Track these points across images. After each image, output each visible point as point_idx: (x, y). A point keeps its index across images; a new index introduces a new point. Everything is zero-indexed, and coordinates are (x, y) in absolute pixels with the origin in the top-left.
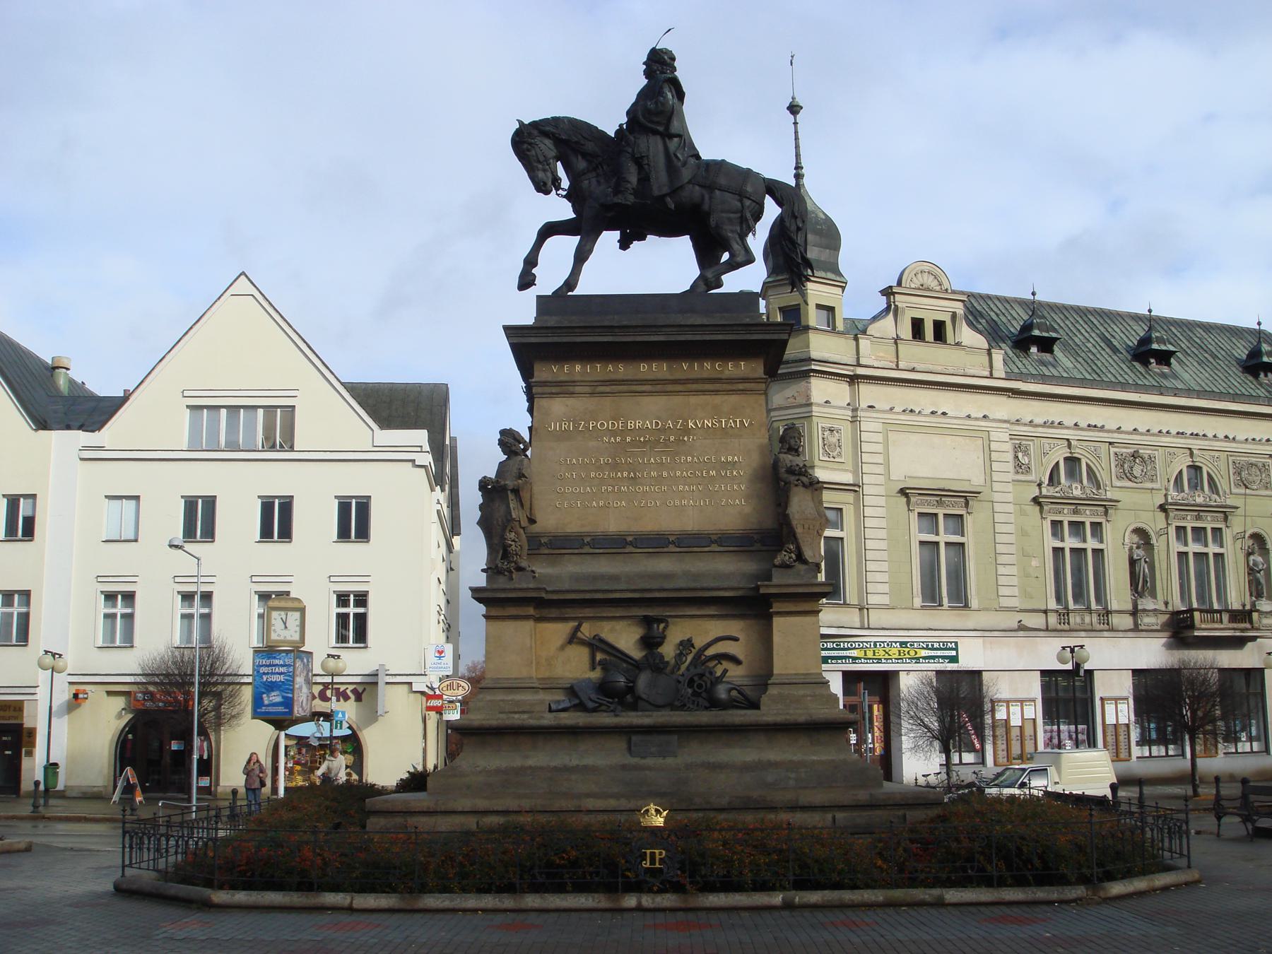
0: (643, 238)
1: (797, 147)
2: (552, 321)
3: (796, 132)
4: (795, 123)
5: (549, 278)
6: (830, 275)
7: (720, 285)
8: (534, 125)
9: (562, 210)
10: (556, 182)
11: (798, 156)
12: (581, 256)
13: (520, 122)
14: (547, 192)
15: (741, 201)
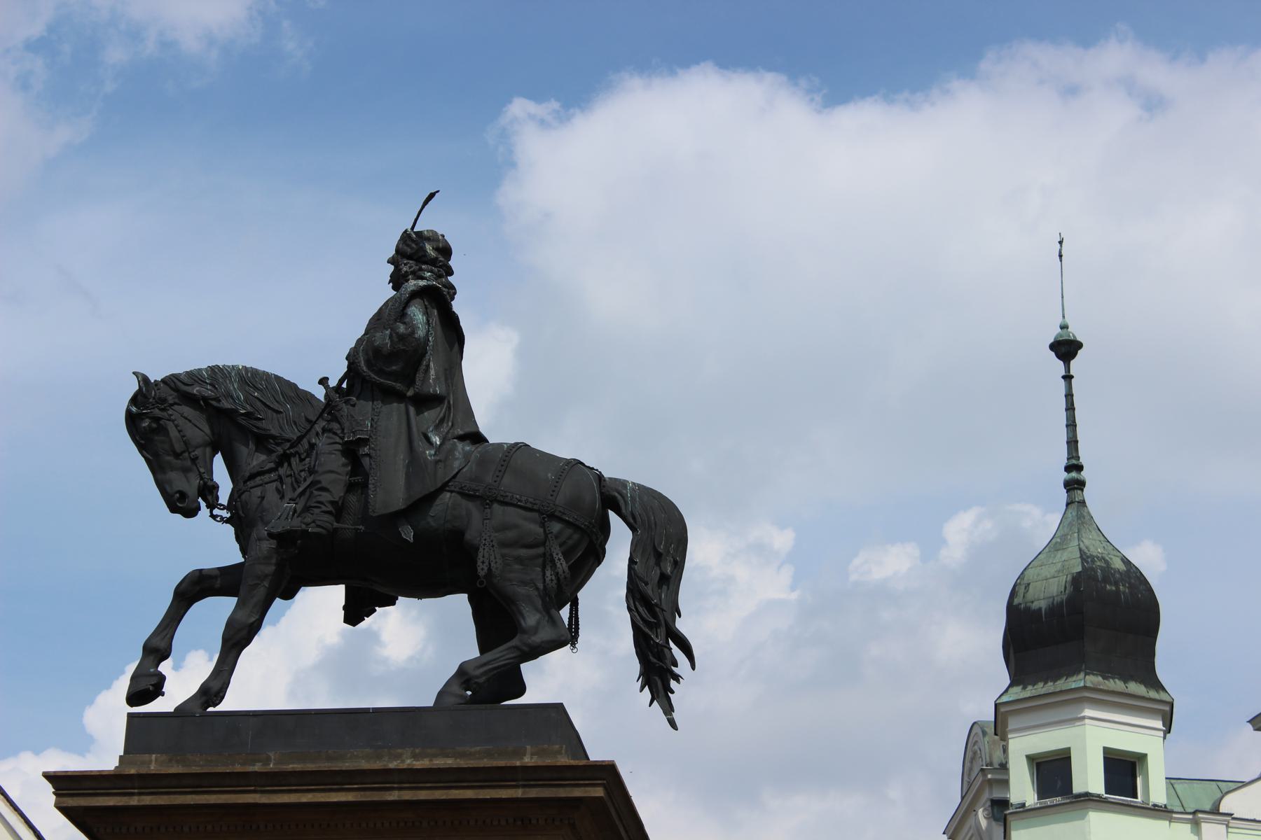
0: (392, 602)
1: (1071, 425)
2: (154, 764)
3: (1069, 396)
4: (1068, 378)
5: (182, 682)
6: (1135, 688)
7: (520, 689)
8: (171, 382)
9: (213, 543)
10: (209, 491)
11: (1073, 443)
12: (237, 639)
13: (144, 380)
14: (191, 512)
15: (543, 525)
